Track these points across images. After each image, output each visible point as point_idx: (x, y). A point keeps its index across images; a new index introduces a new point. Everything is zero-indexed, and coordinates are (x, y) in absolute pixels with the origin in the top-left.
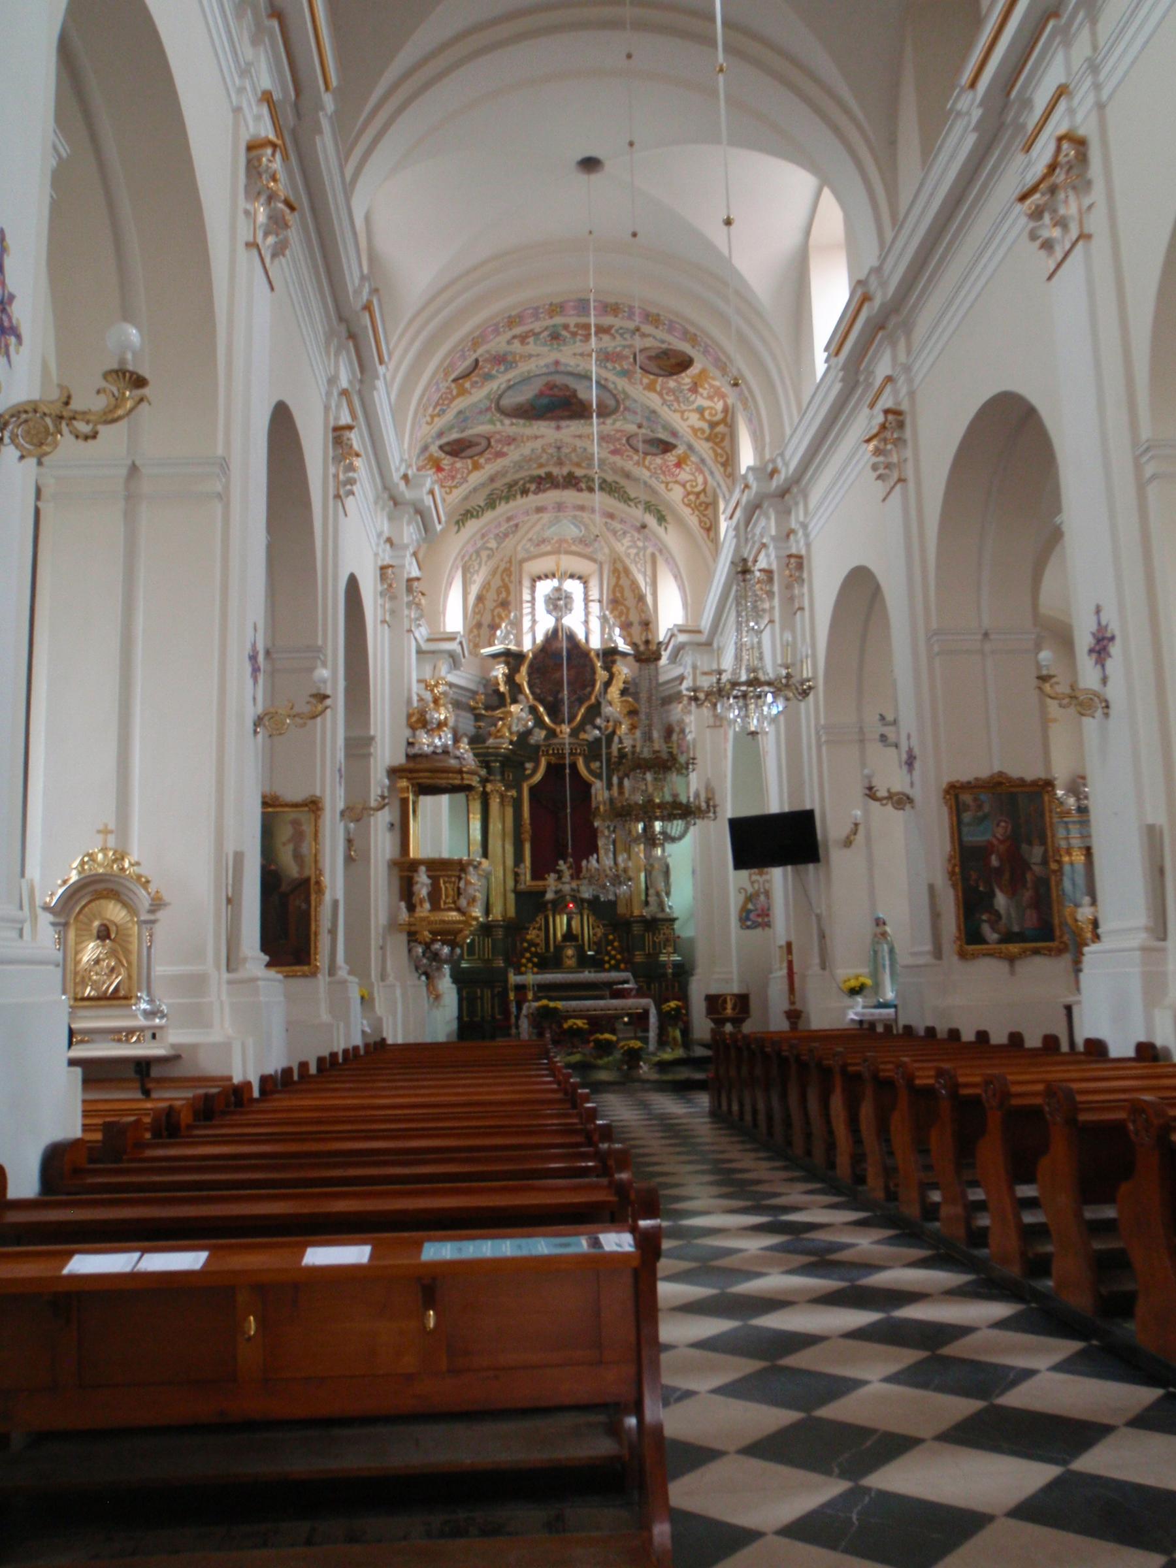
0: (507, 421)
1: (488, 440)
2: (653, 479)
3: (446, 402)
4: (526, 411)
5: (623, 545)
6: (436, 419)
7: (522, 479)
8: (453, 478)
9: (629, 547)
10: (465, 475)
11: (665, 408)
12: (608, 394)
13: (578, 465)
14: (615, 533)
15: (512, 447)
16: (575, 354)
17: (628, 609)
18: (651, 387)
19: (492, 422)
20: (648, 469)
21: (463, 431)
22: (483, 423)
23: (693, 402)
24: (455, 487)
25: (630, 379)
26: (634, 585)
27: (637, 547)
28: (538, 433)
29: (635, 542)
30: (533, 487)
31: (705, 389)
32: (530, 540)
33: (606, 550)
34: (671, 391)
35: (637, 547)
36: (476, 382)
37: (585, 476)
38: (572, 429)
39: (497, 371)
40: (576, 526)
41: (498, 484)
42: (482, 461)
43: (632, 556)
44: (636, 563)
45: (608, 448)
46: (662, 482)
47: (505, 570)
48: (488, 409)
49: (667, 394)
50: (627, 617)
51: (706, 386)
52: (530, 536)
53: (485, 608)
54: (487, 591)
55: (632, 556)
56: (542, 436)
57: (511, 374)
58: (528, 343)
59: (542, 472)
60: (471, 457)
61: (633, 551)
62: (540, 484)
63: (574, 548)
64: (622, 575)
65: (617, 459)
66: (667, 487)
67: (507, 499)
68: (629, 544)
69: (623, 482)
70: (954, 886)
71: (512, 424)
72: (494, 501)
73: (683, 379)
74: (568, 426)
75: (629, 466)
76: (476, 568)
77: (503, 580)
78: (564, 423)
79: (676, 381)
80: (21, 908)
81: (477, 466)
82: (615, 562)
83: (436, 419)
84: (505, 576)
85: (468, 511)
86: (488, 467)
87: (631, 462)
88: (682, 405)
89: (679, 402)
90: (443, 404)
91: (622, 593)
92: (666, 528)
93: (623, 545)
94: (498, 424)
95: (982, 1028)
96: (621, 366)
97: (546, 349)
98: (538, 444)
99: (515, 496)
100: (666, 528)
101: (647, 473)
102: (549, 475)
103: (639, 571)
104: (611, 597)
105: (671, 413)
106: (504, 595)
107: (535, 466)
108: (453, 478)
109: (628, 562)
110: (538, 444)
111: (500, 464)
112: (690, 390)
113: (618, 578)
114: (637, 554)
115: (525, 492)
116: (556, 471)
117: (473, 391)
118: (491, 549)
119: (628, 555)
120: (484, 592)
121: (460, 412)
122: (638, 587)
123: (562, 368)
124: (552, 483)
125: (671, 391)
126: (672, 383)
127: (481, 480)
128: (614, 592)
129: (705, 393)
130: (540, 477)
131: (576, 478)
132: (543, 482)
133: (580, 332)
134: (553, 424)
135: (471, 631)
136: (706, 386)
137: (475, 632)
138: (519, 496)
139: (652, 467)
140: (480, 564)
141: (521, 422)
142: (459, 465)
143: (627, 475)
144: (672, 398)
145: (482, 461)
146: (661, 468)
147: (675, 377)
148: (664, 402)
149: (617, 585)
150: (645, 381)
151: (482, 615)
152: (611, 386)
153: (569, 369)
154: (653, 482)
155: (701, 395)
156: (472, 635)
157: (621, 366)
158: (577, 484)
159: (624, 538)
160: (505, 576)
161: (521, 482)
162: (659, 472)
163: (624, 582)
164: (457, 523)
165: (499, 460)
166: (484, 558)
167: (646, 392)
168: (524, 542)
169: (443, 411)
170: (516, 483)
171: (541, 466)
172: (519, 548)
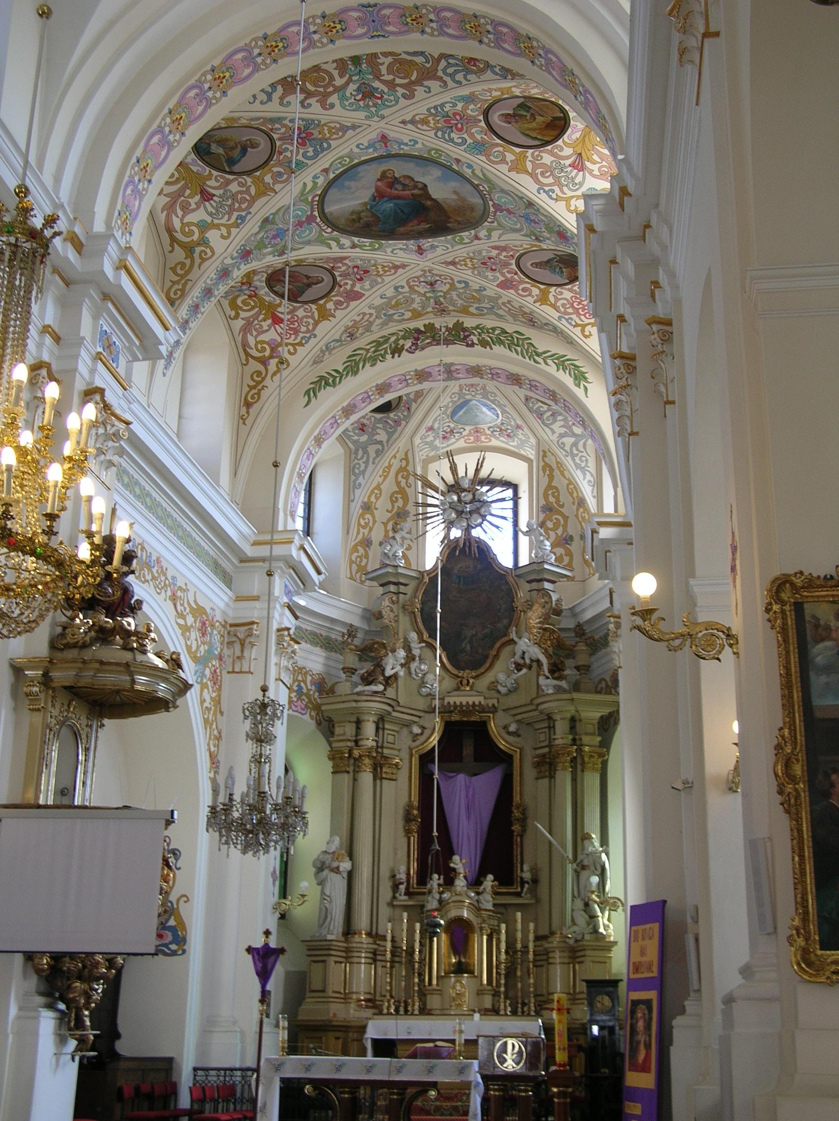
0: (346, 241)
1: (330, 271)
2: (564, 321)
3: (244, 206)
4: (368, 225)
5: (553, 432)
6: (234, 231)
7: (393, 334)
8: (296, 332)
9: (561, 436)
10: (311, 327)
11: (543, 196)
12: (469, 188)
13: (465, 311)
14: (540, 415)
15: (367, 285)
16: (404, 122)
17: (566, 518)
18: (518, 167)
19: (320, 241)
20: (554, 306)
21: (282, 253)
22: (309, 243)
23: (581, 184)
24: (301, 344)
25: (488, 156)
26: (573, 487)
27: (574, 435)
28: (398, 261)
29: (570, 428)
30: (408, 344)
31: (595, 163)
32: (431, 429)
33: (533, 441)
34: (548, 170)
35: (574, 435)
36: (280, 174)
37: (477, 327)
38: (439, 251)
39: (304, 155)
40: (490, 409)
41: (363, 341)
42: (330, 306)
43: (567, 448)
44: (573, 456)
45: (495, 278)
46: (577, 325)
47: (401, 469)
48: (310, 219)
49: (542, 174)
50: (565, 530)
51: (595, 157)
52: (428, 423)
53: (375, 522)
54: (377, 499)
55: (567, 448)
56: (403, 266)
57: (325, 162)
58: (332, 106)
59: (419, 324)
60: (314, 302)
61: (569, 441)
62: (417, 339)
63: (494, 442)
64: (557, 473)
65: (511, 294)
66: (583, 331)
67: (374, 361)
68: (563, 430)
69: (528, 332)
70: (790, 807)
71: (354, 246)
72: (357, 364)
73: (562, 150)
74: (433, 247)
75: (530, 303)
76: (362, 468)
77: (398, 484)
78: (426, 243)
79: (551, 153)
80: (334, 992)
81: (325, 315)
82: (545, 455)
83: (234, 231)
84: (400, 479)
85: (322, 378)
86: (339, 314)
87: (529, 299)
88: (565, 189)
89: (561, 186)
90: (240, 209)
91: (557, 498)
92: (586, 389)
93: (553, 432)
94: (333, 244)
95: (246, 947)
96: (472, 136)
97: (362, 115)
98: (401, 278)
99: (383, 356)
100: (586, 389)
101: (556, 315)
102: (430, 327)
103: (578, 466)
104: (542, 502)
105: (551, 203)
106: (400, 503)
107: (408, 315)
108: (296, 332)
109: (561, 454)
110: (401, 278)
111: (356, 309)
112: (571, 165)
113: (551, 477)
114: (575, 444)
115: (397, 351)
116: (439, 322)
117: (277, 187)
118: (381, 442)
119: (562, 446)
120: (373, 499)
121: (266, 221)
122: (577, 488)
123: (394, 149)
124: (433, 337)
125: (548, 170)
126: (547, 159)
127: (336, 334)
128: (546, 497)
129: (595, 168)
130: (418, 331)
131: (464, 330)
132: (422, 337)
133: (398, 81)
134: (412, 244)
135: (355, 549)
136: (595, 157)
137: (361, 550)
138: (389, 356)
139: (559, 304)
140: (367, 463)
141: (367, 241)
142: (300, 313)
143: (532, 321)
144: (551, 180)
145: (330, 306)
146: (572, 306)
147: (549, 148)
148: (541, 187)
149: (549, 487)
150: (510, 157)
151: (371, 529)
152: (468, 172)
153: (406, 149)
154: (563, 325)
155: (591, 172)
156: (356, 554)
157: (472, 136)
158: (466, 337)
159: (555, 421)
160: (400, 479)
161: (393, 339)
162: (570, 310)
163: (559, 482)
164: (307, 393)
165: (353, 304)
166: (372, 455)
167: (513, 175)
168: (422, 431)
169: (243, 218)
170: (386, 339)
171: (416, 315)
172: (417, 441)
